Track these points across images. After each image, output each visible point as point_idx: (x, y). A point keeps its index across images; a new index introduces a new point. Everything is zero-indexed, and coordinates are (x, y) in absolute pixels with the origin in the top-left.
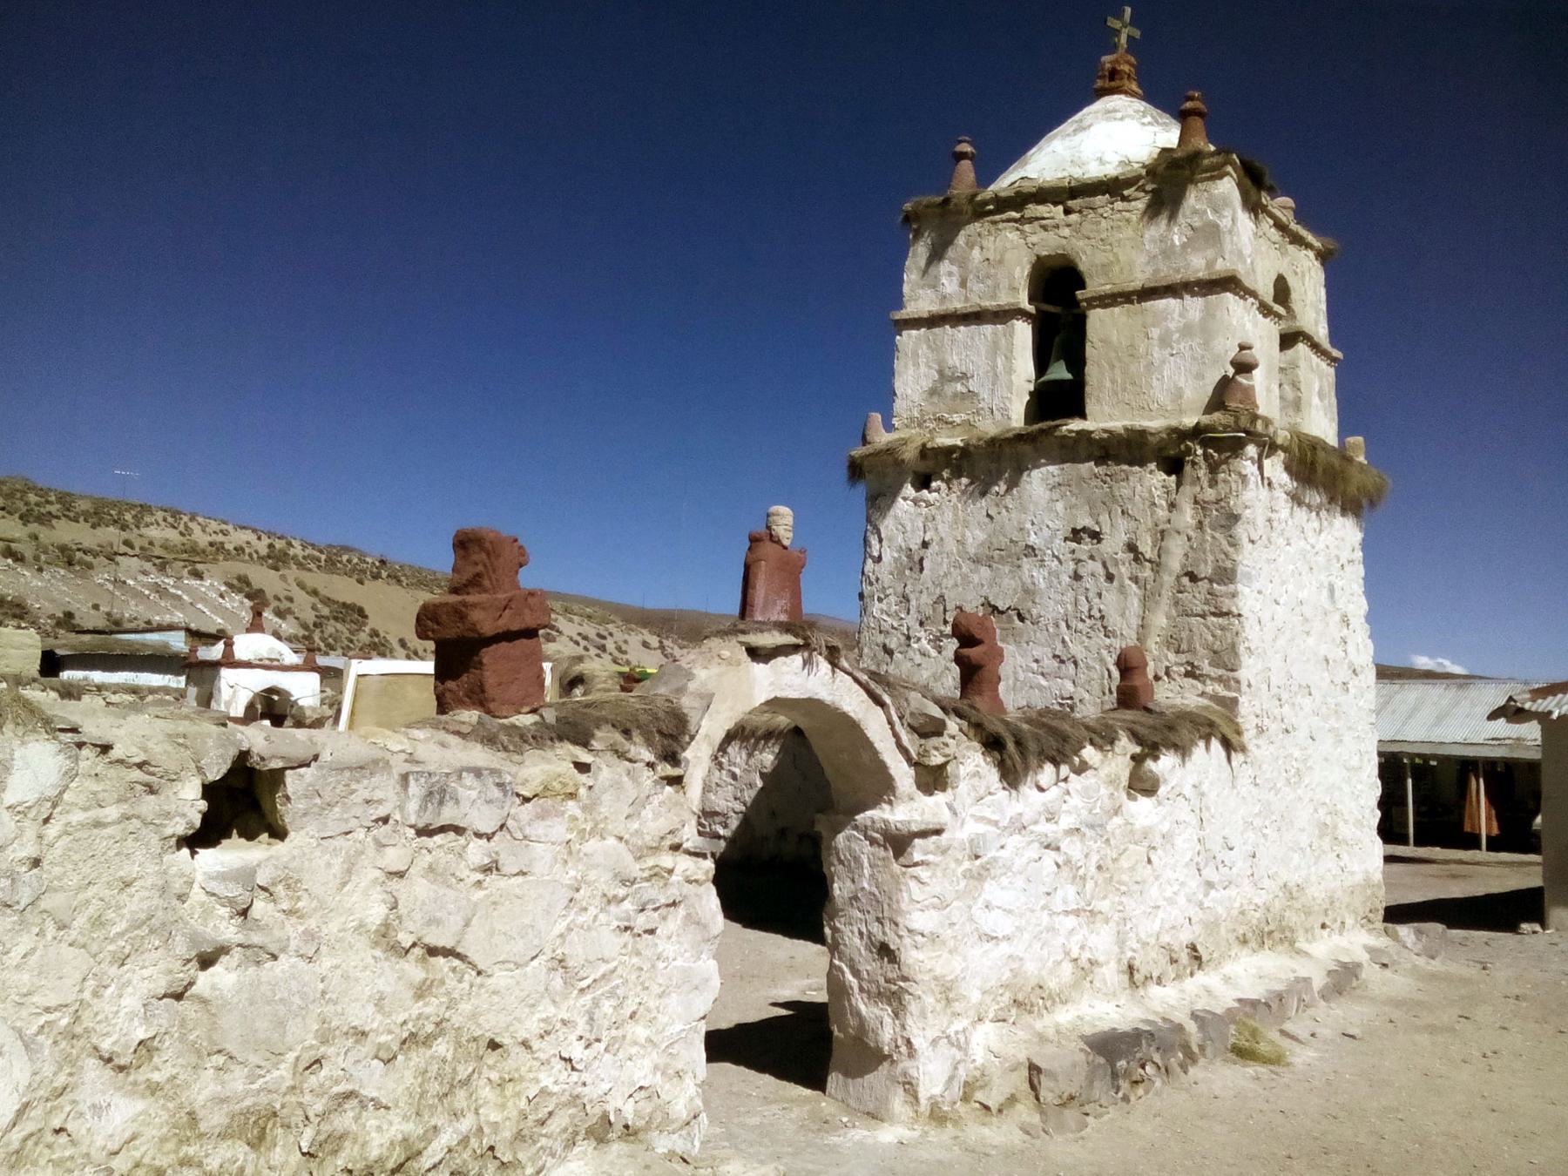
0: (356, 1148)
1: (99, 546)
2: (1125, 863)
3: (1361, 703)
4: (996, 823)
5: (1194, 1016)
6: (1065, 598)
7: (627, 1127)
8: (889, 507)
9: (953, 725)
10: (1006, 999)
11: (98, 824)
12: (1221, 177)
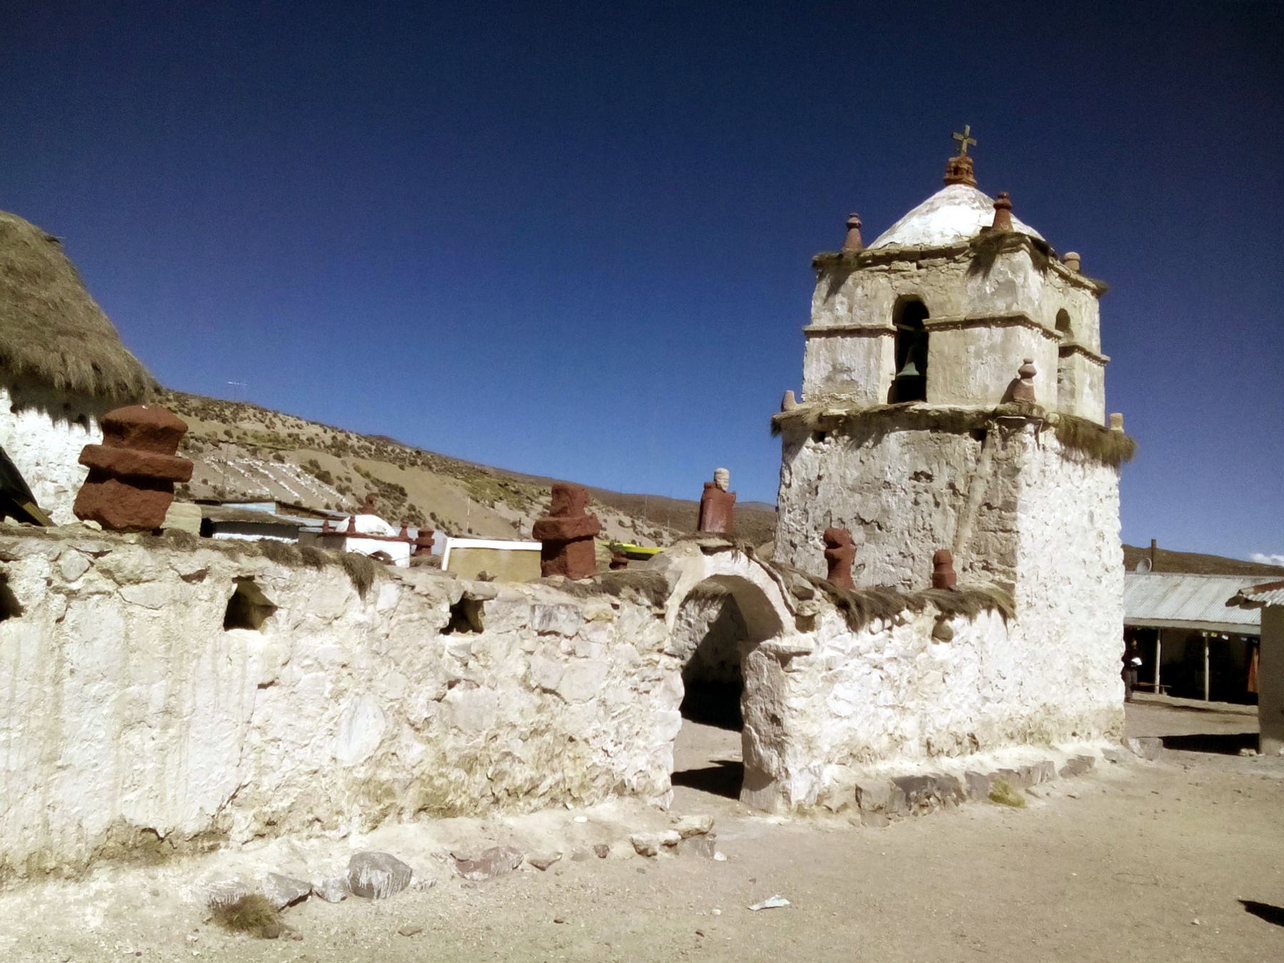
0: (511, 779)
1: (206, 434)
2: (927, 681)
3: (1111, 591)
4: (843, 651)
5: (967, 775)
6: (908, 516)
7: (633, 790)
8: (797, 453)
9: (818, 593)
10: (846, 752)
11: (410, 621)
12: (1018, 251)
